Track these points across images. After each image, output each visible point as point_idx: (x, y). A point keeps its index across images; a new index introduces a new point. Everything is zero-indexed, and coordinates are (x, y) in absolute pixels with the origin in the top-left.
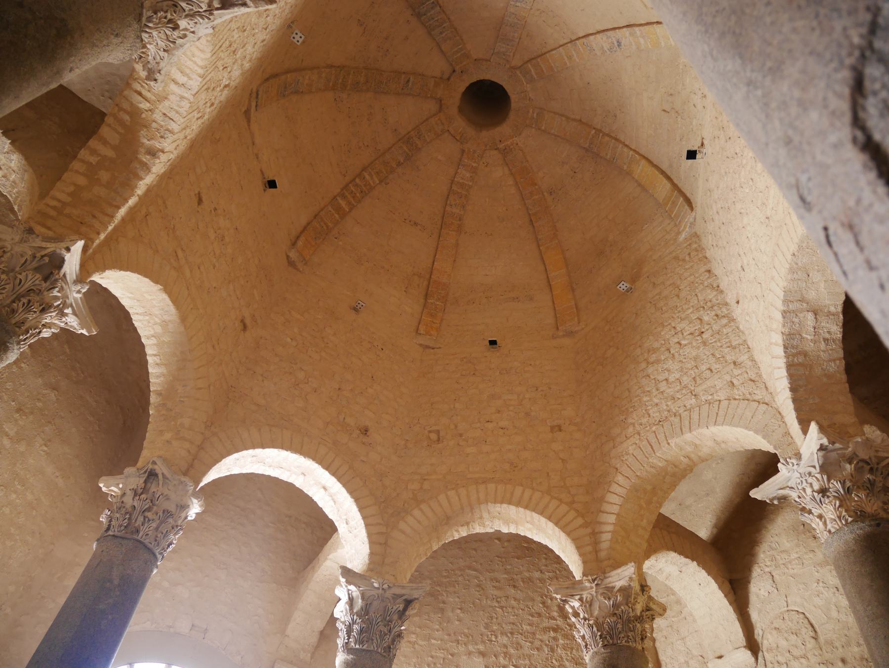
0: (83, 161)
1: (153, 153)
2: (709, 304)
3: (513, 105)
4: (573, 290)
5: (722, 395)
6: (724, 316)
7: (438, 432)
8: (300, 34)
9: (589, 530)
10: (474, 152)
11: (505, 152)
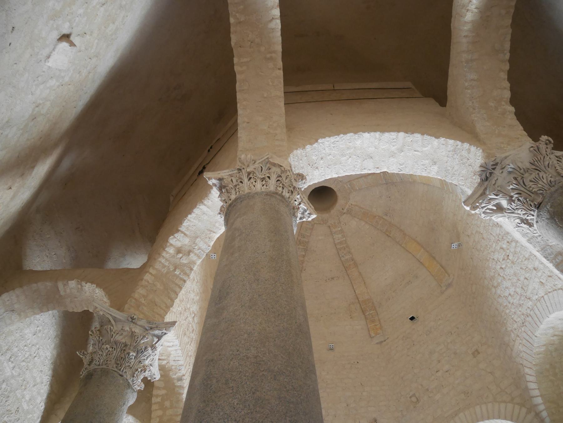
0: (155, 403)
1: (180, 379)
2: (500, 237)
3: (335, 189)
4: (434, 258)
5: (541, 293)
6: (511, 241)
7: (414, 395)
8: (213, 255)
9: (533, 414)
10: (335, 223)
11: (349, 212)
